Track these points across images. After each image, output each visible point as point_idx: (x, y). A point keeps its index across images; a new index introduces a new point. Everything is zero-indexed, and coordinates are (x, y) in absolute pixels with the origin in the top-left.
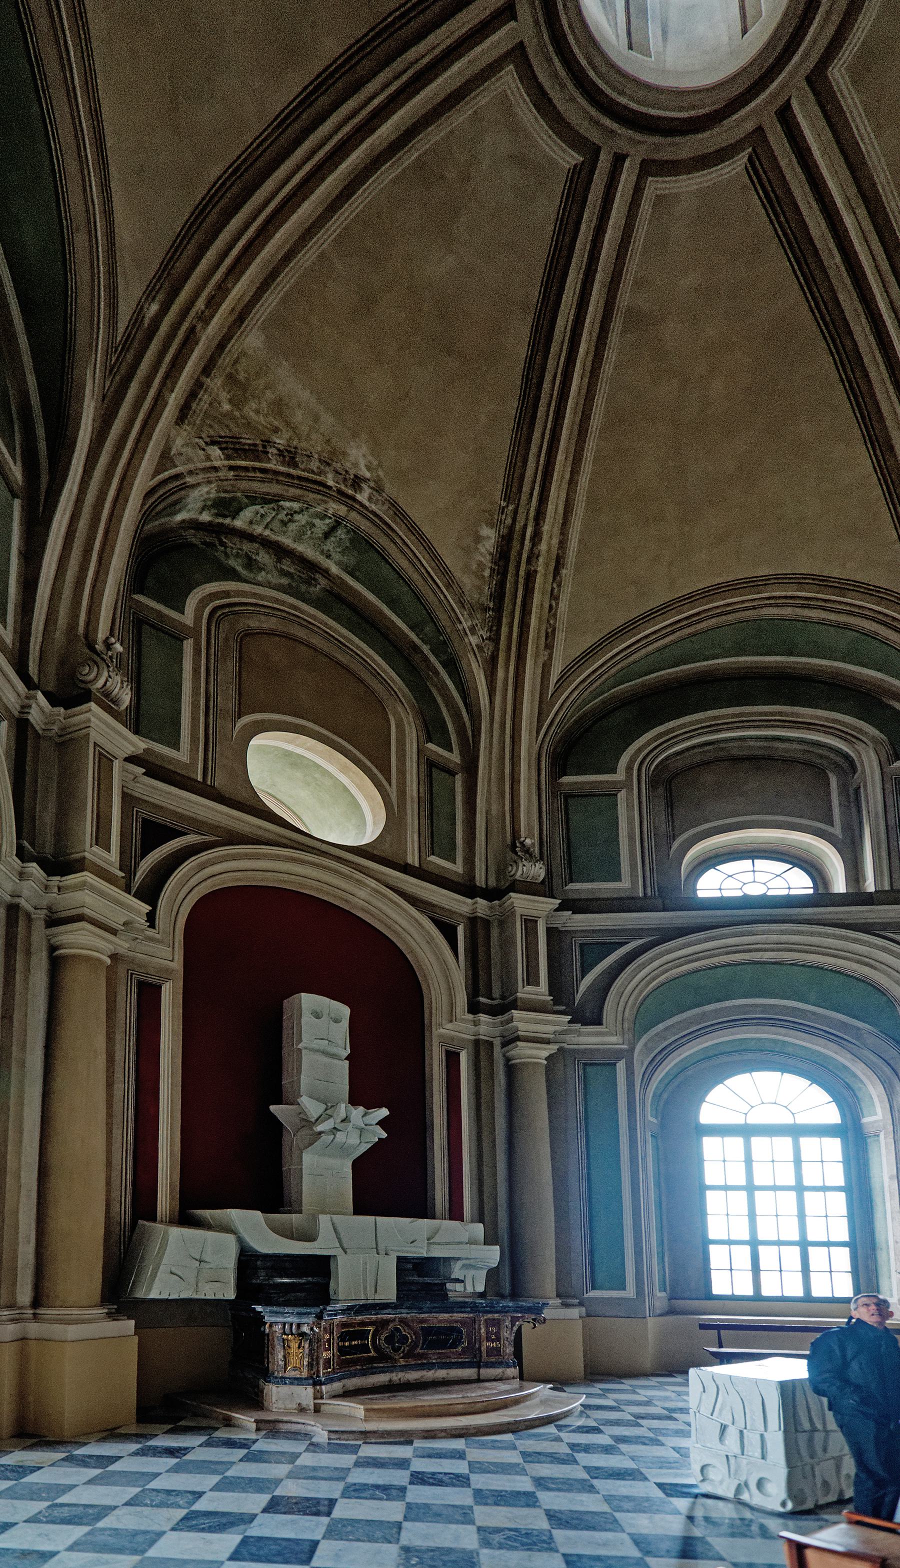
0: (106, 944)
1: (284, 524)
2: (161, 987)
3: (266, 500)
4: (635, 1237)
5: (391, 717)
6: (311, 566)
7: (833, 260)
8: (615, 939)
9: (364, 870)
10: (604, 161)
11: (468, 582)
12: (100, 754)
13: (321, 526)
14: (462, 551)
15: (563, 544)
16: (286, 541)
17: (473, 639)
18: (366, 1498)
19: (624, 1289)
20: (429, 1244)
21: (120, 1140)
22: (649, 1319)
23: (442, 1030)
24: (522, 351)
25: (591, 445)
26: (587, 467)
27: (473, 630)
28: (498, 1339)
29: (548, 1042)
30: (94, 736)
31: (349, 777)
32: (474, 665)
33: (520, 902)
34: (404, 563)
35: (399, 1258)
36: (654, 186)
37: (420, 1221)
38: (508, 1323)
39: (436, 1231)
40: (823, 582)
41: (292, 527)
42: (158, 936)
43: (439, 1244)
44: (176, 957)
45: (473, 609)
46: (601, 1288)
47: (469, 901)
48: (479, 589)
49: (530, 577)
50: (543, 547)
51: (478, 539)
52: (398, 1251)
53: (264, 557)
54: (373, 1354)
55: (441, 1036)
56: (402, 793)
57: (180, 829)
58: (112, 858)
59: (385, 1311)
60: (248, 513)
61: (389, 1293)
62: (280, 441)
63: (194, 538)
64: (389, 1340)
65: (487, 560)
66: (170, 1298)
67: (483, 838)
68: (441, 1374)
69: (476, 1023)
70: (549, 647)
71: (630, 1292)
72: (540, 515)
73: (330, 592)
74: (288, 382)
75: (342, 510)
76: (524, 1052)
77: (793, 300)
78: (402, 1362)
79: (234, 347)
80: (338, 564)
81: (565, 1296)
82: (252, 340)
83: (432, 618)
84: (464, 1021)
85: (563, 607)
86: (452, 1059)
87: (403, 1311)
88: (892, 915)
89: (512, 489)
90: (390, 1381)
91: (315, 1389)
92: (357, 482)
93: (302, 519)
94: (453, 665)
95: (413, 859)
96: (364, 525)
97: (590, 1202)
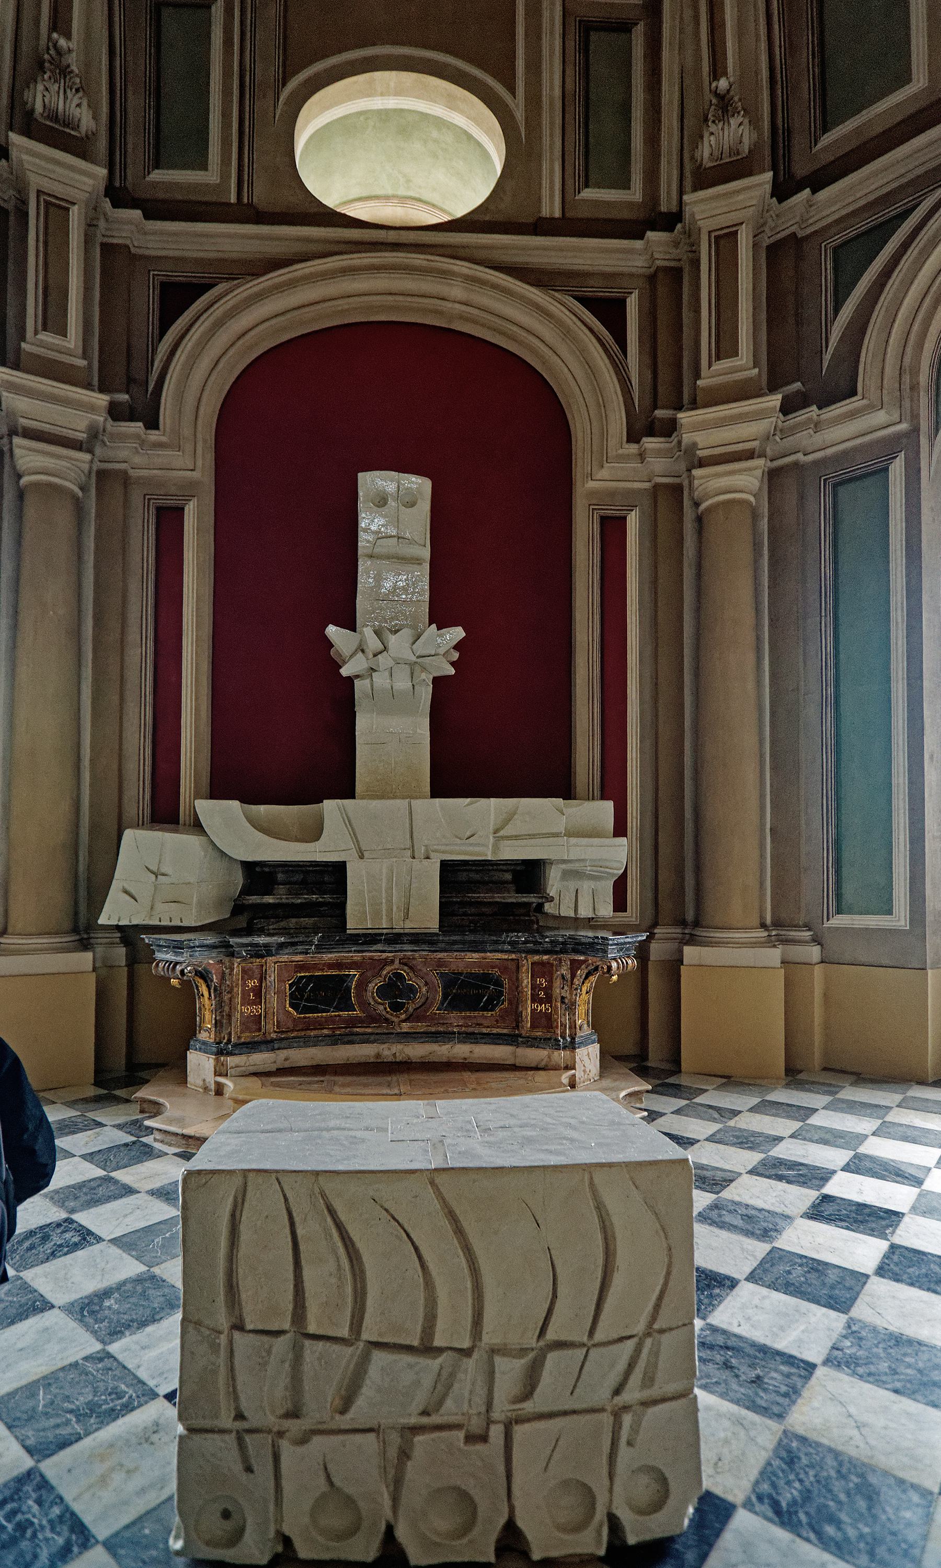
0: (58, 462)
2: (183, 509)
4: (911, 810)
8: (892, 211)
9: (462, 253)
12: (47, 203)
18: (842, 1228)
19: (890, 912)
20: (498, 839)
21: (136, 721)
22: (930, 972)
23: (591, 484)
28: (549, 999)
29: (750, 455)
30: (35, 182)
31: (462, 112)
33: (708, 209)
35: (444, 864)
37: (483, 801)
38: (565, 970)
39: (509, 819)
42: (164, 439)
43: (516, 837)
44: (199, 463)
46: (850, 912)
47: (638, 244)
52: (443, 852)
54: (357, 1013)
55: (592, 493)
56: (534, 101)
57: (203, 281)
58: (70, 343)
59: (375, 947)
61: (427, 916)
64: (383, 992)
66: (120, 924)
67: (675, 124)
68: (461, 1051)
69: (642, 456)
71: (900, 918)
76: (713, 484)
78: (405, 1027)
81: (779, 928)
84: (621, 458)
86: (612, 529)
87: (406, 947)
90: (378, 1056)
91: (217, 1060)
95: (551, 207)
97: (838, 752)
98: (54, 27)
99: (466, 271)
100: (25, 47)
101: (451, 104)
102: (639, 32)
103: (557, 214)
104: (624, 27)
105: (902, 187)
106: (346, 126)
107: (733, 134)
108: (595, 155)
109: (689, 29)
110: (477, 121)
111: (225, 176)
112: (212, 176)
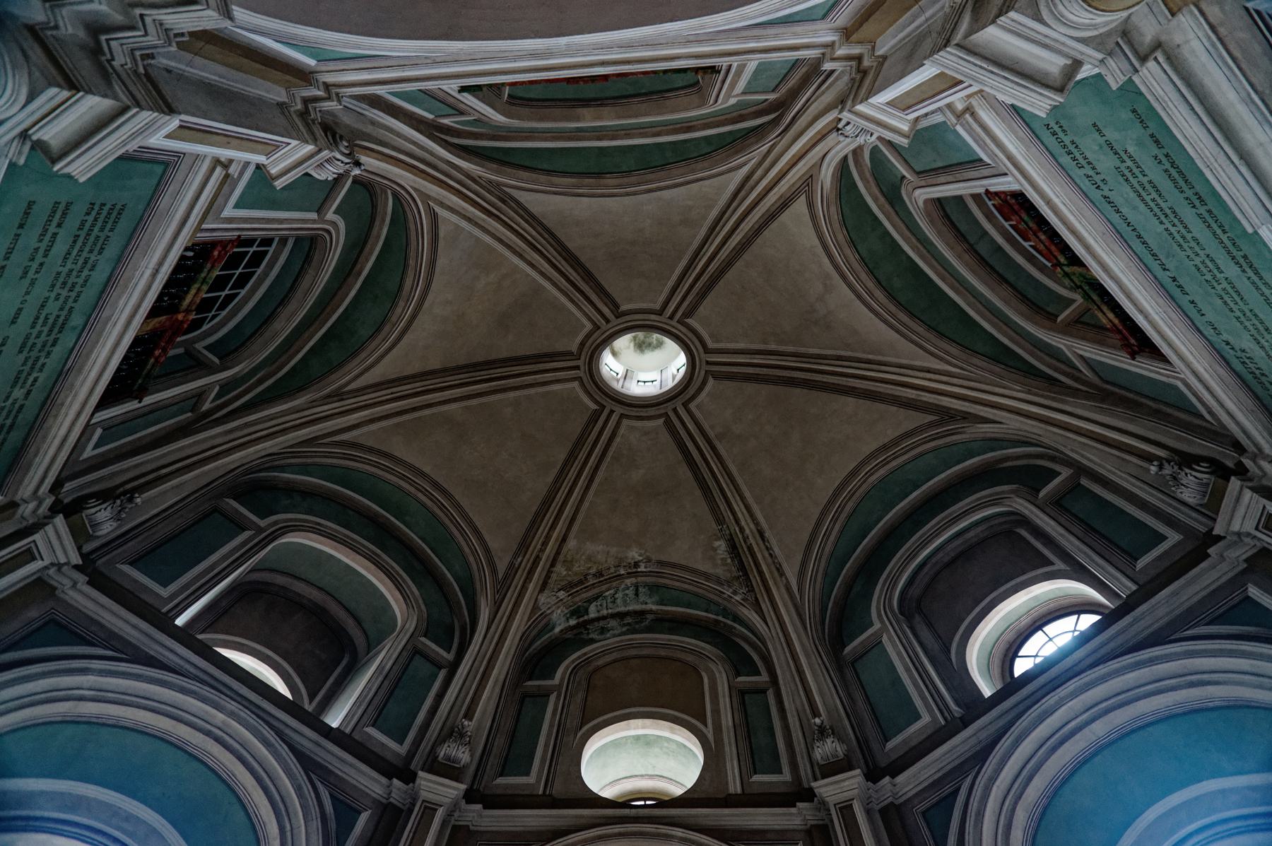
1: (614, 602)
3: (596, 598)
5: (704, 674)
6: (641, 614)
7: (765, 371)
8: (947, 790)
10: (671, 414)
11: (720, 571)
13: (631, 592)
14: (717, 561)
15: (757, 524)
16: (622, 609)
17: (736, 597)
24: (689, 474)
25: (739, 480)
26: (744, 488)
27: (735, 593)
32: (746, 612)
34: (678, 584)
36: (692, 406)
40: (884, 448)
41: (618, 601)
45: (729, 583)
47: (793, 810)
48: (730, 571)
49: (750, 548)
50: (747, 531)
51: (715, 550)
53: (613, 623)
56: (718, 729)
60: (592, 608)
62: (593, 571)
63: (569, 635)
65: (726, 555)
70: (782, 574)
72: (737, 521)
73: (657, 620)
74: (590, 547)
75: (633, 580)
77: (766, 389)
79: (565, 550)
80: (653, 603)
82: (572, 543)
83: (710, 601)
85: (777, 550)
88: (1161, 612)
89: (720, 521)
92: (636, 565)
93: (619, 595)
94: (737, 618)
95: (735, 787)
96: (649, 580)
98: (465, 717)
99: (680, 834)
100: (448, 723)
101: (673, 731)
102: (771, 695)
103: (739, 791)
104: (764, 692)
105: (945, 775)
106: (616, 744)
107: (828, 748)
108: (758, 753)
109: (1232, 79)
110: (689, 740)
111: (538, 781)
112: (532, 780)
